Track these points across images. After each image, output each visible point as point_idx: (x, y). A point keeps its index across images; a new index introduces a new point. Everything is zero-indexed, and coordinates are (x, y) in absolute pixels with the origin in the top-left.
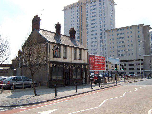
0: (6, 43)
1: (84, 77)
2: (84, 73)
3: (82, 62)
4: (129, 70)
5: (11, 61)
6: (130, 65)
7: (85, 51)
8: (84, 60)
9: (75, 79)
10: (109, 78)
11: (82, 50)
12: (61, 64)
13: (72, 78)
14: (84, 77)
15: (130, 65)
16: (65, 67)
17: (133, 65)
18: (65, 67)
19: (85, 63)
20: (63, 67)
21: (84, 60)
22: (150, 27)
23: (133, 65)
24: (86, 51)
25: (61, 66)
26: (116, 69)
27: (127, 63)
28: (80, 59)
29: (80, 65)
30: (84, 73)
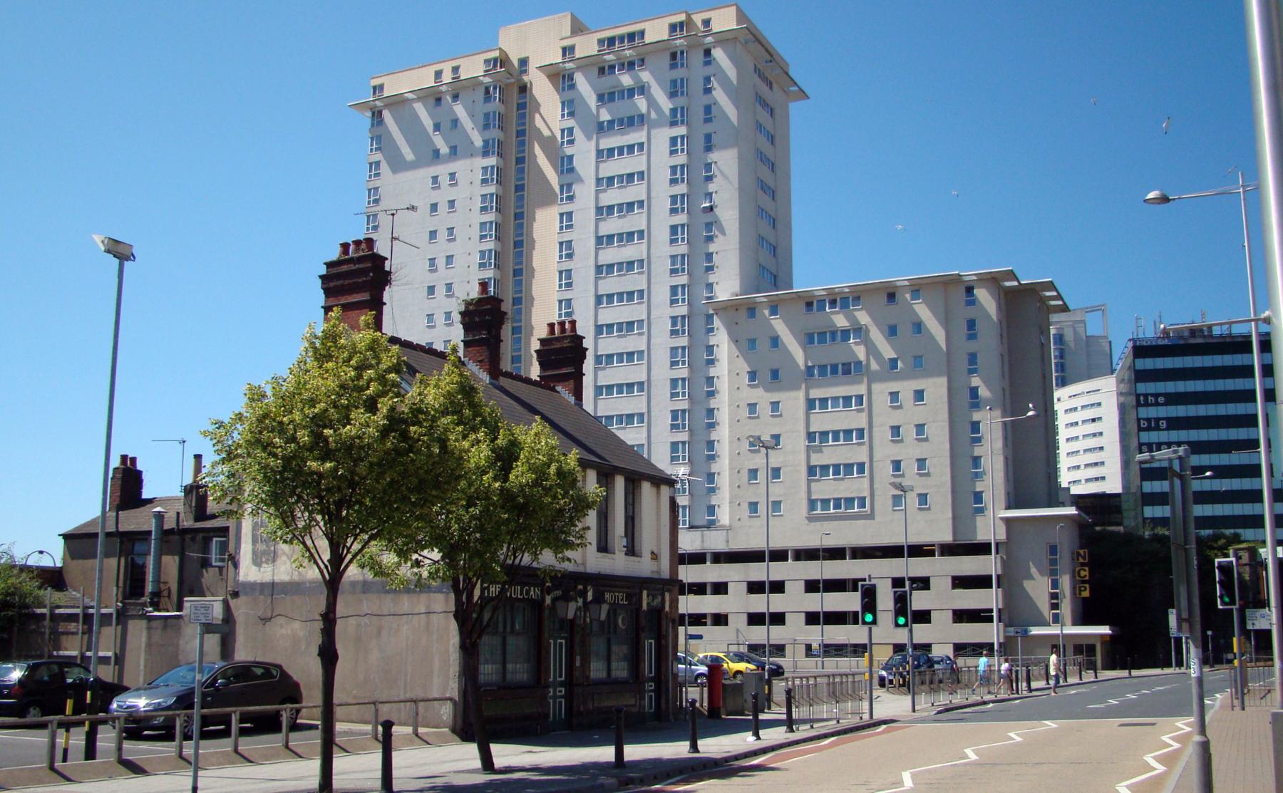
0: (819, 702)
1: (648, 669)
2: (649, 644)
3: (643, 567)
4: (955, 622)
5: (61, 541)
6: (755, 588)
7: (658, 493)
8: (655, 556)
9: (600, 683)
10: (511, 562)
11: (646, 487)
12: (530, 585)
13: (588, 677)
14: (648, 669)
15: (755, 588)
16: (548, 600)
17: (778, 587)
18: (548, 600)
19: (658, 572)
20: (537, 605)
21: (655, 556)
22: (1059, 297)
23: (778, 587)
24: (665, 490)
25: (528, 593)
26: (869, 618)
27: (941, 569)
28: (632, 550)
29: (634, 585)
30: (649, 644)
